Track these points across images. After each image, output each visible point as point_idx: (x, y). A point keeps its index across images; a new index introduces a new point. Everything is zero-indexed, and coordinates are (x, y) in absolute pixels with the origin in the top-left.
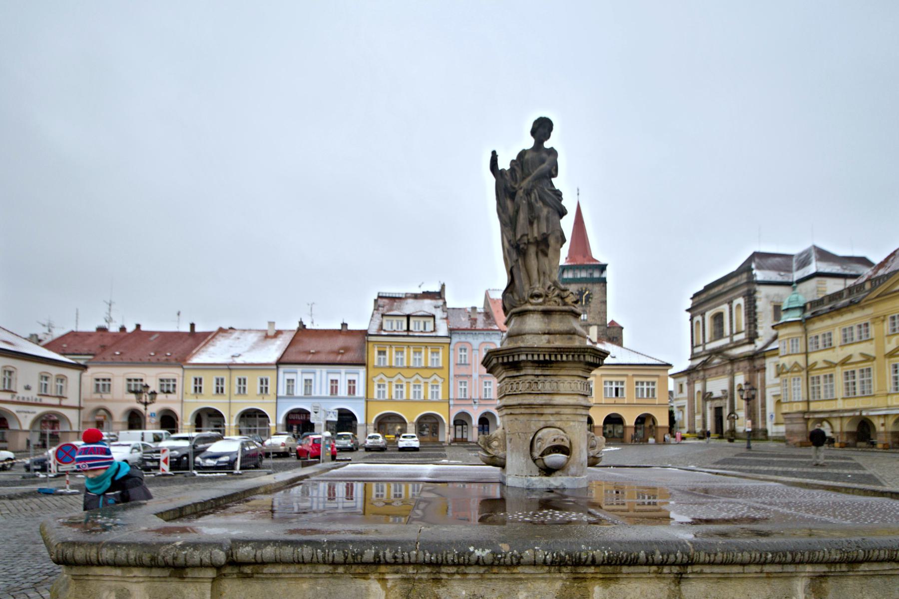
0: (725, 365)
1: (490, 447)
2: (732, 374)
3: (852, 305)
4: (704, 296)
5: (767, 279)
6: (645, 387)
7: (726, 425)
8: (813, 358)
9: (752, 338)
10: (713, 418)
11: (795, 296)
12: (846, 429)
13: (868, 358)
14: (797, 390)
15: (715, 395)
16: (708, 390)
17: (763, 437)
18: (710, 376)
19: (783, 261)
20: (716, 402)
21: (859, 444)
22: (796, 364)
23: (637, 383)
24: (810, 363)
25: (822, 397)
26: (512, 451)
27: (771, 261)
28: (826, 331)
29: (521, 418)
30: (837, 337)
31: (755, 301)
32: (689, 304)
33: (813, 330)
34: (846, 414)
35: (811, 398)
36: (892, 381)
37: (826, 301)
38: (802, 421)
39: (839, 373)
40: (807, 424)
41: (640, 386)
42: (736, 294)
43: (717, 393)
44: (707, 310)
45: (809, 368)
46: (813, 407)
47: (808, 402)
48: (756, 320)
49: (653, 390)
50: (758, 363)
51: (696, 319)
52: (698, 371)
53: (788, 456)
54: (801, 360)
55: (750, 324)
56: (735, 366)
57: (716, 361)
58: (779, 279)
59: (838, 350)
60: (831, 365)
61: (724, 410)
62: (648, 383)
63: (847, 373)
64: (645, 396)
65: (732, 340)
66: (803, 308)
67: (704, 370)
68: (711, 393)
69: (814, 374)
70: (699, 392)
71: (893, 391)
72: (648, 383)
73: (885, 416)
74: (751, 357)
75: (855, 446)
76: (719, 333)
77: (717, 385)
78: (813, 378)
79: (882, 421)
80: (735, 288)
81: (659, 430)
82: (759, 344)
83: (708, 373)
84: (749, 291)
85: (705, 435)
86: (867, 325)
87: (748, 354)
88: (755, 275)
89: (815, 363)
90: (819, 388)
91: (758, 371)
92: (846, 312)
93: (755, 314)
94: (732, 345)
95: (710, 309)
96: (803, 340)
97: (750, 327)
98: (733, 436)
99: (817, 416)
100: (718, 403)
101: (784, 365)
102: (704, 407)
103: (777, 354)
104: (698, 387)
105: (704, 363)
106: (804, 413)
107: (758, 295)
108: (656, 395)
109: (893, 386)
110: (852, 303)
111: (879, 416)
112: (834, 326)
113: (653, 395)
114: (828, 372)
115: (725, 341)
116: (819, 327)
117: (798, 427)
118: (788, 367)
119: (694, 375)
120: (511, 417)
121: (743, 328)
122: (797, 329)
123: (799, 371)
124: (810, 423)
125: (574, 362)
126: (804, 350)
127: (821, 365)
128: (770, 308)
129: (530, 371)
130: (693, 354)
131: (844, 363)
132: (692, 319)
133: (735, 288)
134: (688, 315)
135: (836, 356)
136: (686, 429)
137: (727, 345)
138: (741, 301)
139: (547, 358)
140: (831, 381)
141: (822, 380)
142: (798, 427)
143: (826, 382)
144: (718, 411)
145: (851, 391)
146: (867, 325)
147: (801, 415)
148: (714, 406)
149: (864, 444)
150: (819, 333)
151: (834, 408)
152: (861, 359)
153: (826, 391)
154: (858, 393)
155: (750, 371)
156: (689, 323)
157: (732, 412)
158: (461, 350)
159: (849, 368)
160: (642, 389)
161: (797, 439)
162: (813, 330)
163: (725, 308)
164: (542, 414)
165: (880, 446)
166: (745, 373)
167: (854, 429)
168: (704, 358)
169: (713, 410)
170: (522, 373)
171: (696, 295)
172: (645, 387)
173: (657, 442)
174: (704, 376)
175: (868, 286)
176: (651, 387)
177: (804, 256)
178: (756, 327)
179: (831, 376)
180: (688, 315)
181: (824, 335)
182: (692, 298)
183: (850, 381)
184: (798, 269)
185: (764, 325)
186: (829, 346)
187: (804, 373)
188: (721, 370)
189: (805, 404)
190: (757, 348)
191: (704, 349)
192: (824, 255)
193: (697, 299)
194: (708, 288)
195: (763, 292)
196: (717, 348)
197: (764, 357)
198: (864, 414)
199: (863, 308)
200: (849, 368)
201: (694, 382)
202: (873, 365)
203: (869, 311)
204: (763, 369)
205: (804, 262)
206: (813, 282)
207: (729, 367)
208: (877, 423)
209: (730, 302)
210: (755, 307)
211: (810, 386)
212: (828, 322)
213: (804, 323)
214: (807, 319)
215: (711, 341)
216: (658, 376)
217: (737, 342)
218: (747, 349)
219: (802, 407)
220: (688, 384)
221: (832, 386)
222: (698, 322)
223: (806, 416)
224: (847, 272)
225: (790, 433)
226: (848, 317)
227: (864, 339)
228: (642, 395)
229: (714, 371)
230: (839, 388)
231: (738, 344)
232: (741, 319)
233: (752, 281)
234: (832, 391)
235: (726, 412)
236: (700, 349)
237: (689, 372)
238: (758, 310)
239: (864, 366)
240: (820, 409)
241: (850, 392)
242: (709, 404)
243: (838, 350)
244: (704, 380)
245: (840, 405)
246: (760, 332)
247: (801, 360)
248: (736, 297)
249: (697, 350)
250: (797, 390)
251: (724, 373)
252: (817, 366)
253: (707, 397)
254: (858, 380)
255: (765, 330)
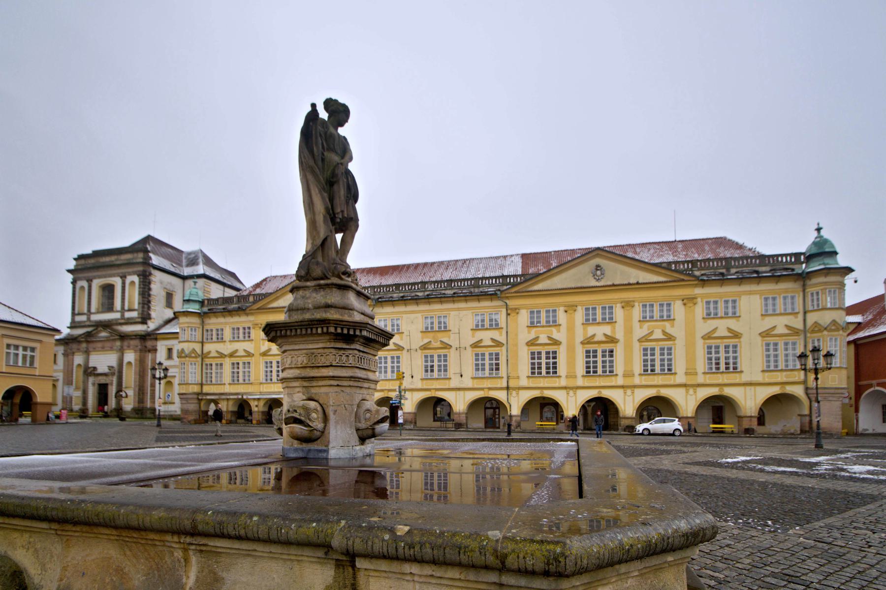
0: (114, 340)
1: (310, 420)
2: (121, 351)
3: (240, 311)
4: (92, 261)
5: (162, 266)
6: (21, 352)
7: (112, 403)
8: (208, 347)
9: (145, 319)
10: (96, 394)
11: (195, 290)
12: (231, 409)
13: (249, 354)
14: (193, 373)
15: (100, 371)
16: (91, 365)
17: (152, 416)
18: (95, 349)
19: (174, 254)
20: (100, 378)
21: (239, 421)
22: (194, 350)
23: (8, 346)
24: (205, 351)
25: (214, 382)
26: (337, 423)
27: (165, 250)
28: (219, 327)
29: (348, 390)
30: (228, 334)
31: (150, 283)
32: (72, 265)
33: (209, 324)
34: (232, 397)
35: (204, 382)
36: (264, 373)
37: (220, 301)
38: (196, 401)
39: (227, 362)
40: (200, 404)
41: (12, 351)
42: (130, 270)
43: (102, 368)
44: (95, 278)
45: (204, 356)
46: (206, 389)
47: (202, 385)
48: (149, 302)
49: (32, 357)
50: (149, 344)
51: (80, 283)
52: (80, 342)
53: (184, 432)
54: (197, 347)
55: (143, 304)
56: (126, 343)
57: (104, 334)
58: (172, 269)
59: (228, 344)
60: (222, 355)
61: (110, 387)
62: (25, 349)
63: (233, 364)
64: (20, 364)
65: (123, 315)
66: (202, 303)
67: (88, 342)
68: (95, 368)
69: (208, 361)
70: (79, 365)
71: (264, 381)
72: (25, 349)
73: (259, 399)
74: (144, 337)
75: (236, 423)
76: (109, 307)
77: (103, 361)
78: (207, 365)
79: (256, 403)
80: (129, 264)
81: (39, 407)
82: (152, 325)
83: (91, 345)
84: (144, 271)
85: (83, 414)
86: (249, 328)
87: (140, 333)
88: (150, 258)
89: (209, 352)
90: (238, 373)
91: (149, 351)
92: (235, 315)
93: (149, 295)
94: (123, 321)
95: (99, 277)
96: (201, 330)
97: (143, 307)
98: (119, 413)
99: (209, 397)
100: (103, 380)
101: (183, 350)
102: (85, 383)
103: (177, 338)
104: (78, 359)
105: (89, 334)
106: (198, 394)
107: (152, 278)
108: (36, 364)
109: (264, 378)
110: (240, 309)
111: (254, 399)
112: (226, 323)
113: (32, 363)
114: (219, 361)
115: (117, 315)
116: (214, 323)
117: (193, 407)
118: (187, 352)
119: (74, 346)
120: (336, 389)
121: (136, 306)
122: (196, 320)
123: (196, 357)
124: (202, 403)
125: (296, 335)
126: (201, 340)
127: (213, 354)
128: (164, 294)
129: (358, 347)
130: (73, 321)
131: (231, 355)
132: (74, 282)
133: (129, 264)
134: (70, 277)
135: (226, 348)
136: (60, 406)
137: (117, 320)
138: (136, 279)
139: (345, 331)
140: (221, 368)
141: (214, 367)
142: (193, 407)
143: (217, 369)
144: (103, 390)
145: (269, 378)
146: (249, 328)
147: (196, 396)
148: (97, 382)
149: (243, 421)
150: (214, 328)
151: (222, 391)
152: (244, 354)
153: (216, 377)
154: (241, 381)
155: (141, 351)
156: (71, 286)
157: (119, 390)
158: (8, 346)
159: (235, 360)
160: (17, 355)
161: (191, 418)
162: (209, 324)
163: (117, 282)
164: (361, 387)
165: (254, 422)
166: (135, 351)
167: (236, 409)
168: (89, 329)
169: (96, 386)
170: (352, 347)
171: (81, 257)
172: (21, 352)
173: (34, 421)
174: (87, 348)
175: (251, 299)
176: (29, 353)
177: (193, 256)
178: (149, 308)
179: (221, 365)
180: (70, 277)
181: (217, 330)
182: (75, 259)
183: (236, 370)
184: (187, 266)
185: (157, 308)
186: (220, 340)
187: (199, 359)
188: (108, 344)
189: (199, 387)
190: (149, 330)
191: (89, 319)
192: (209, 262)
193: (82, 262)
194: (97, 254)
195: (158, 278)
196: (105, 321)
197: (156, 339)
198: (245, 397)
199: (247, 315)
200: (235, 360)
201: (73, 353)
202: (252, 360)
203: (251, 318)
204: (155, 350)
205: (193, 262)
206: (201, 282)
207: (118, 343)
208: (253, 404)
209: (123, 277)
210: (150, 289)
211: (204, 371)
212: (221, 320)
213: (202, 316)
214: (205, 313)
215: (98, 312)
216: (40, 341)
217: (128, 319)
218: (139, 328)
219: (196, 389)
220: (65, 355)
221: (221, 373)
222: (82, 288)
223: (199, 397)
224: (225, 281)
225: (185, 411)
226: (236, 319)
227: (236, 339)
228: (16, 361)
229: (99, 345)
230: (227, 377)
231: (130, 322)
232: (134, 297)
233: (147, 262)
234: (221, 377)
235: (112, 390)
236: (84, 318)
237: (67, 341)
238: (152, 293)
239: (247, 360)
240: (212, 391)
241: (235, 381)
242: (91, 379)
243: (228, 344)
244: (87, 353)
245: (227, 389)
246: (153, 314)
247: (197, 347)
248: (130, 274)
249: (78, 318)
250: (193, 373)
251: (111, 349)
252: (237, 354)
253: (89, 371)
254: (241, 370)
255: (159, 313)
